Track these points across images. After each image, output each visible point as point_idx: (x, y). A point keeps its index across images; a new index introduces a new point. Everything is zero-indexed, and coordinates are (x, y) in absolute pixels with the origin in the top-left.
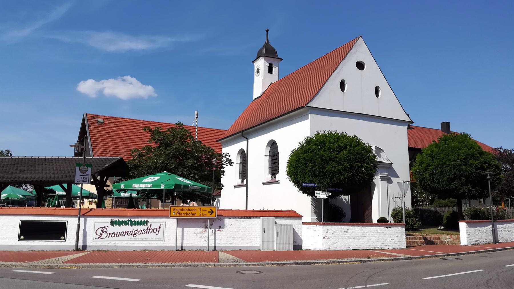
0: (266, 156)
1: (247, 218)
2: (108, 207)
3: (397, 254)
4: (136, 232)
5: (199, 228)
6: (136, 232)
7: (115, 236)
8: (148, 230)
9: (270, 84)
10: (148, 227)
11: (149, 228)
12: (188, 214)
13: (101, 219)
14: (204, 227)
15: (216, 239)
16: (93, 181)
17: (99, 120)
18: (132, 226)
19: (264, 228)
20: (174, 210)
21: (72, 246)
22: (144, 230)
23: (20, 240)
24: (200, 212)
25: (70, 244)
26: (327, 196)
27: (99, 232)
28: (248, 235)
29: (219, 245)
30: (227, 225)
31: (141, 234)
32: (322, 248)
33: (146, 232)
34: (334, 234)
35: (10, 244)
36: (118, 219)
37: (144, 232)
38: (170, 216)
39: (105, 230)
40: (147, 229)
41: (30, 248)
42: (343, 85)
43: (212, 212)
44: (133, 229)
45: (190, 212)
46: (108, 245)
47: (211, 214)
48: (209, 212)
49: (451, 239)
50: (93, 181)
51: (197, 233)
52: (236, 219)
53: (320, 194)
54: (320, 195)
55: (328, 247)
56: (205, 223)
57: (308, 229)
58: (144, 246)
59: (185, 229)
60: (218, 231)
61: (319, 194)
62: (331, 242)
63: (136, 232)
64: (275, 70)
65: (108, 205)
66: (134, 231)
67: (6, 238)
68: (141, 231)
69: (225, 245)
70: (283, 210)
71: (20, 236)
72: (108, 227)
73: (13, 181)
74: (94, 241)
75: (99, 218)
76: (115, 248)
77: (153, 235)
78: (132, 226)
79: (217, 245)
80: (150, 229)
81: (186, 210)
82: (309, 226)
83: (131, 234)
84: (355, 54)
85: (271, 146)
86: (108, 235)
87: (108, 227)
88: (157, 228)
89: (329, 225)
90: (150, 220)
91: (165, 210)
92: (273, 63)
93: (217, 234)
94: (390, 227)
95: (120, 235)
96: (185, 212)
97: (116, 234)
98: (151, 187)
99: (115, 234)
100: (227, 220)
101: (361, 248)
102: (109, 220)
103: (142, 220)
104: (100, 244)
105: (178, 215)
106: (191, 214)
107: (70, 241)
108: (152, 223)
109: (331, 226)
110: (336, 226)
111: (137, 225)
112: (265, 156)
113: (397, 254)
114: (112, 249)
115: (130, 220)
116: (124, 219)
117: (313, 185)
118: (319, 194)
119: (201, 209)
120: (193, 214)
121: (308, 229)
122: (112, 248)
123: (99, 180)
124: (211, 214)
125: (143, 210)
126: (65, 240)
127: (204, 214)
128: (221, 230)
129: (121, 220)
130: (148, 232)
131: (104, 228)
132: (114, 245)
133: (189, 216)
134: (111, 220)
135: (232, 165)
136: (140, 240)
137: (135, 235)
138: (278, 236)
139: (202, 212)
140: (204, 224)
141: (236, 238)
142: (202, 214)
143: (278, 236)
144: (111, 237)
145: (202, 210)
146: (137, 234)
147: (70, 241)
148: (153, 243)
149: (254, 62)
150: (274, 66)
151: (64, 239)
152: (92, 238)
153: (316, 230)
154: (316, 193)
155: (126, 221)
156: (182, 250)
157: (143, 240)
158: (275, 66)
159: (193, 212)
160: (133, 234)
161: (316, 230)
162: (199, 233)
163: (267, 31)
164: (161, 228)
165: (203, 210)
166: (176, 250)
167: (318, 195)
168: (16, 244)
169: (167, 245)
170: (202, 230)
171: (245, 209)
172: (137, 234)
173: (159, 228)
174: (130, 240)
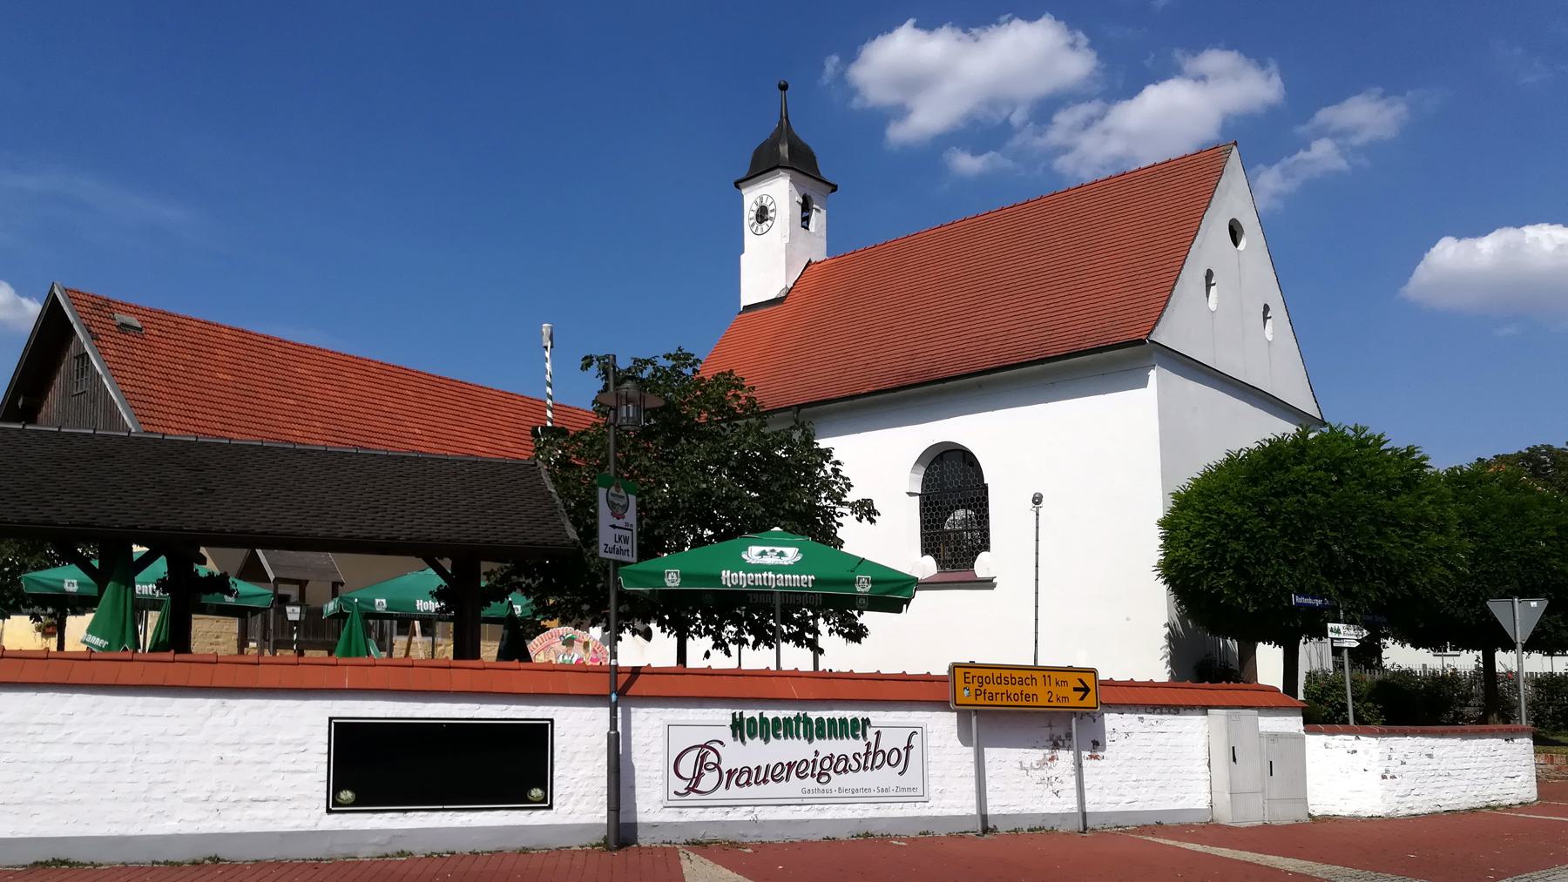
0: (910, 494)
1: (1169, 713)
2: (213, 646)
4: (828, 761)
5: (1035, 747)
6: (828, 761)
7: (752, 781)
8: (871, 757)
9: (807, 265)
10: (868, 745)
11: (872, 750)
12: (1012, 697)
13: (691, 710)
14: (1047, 744)
15: (1086, 786)
16: (134, 546)
17: (121, 318)
18: (810, 740)
19: (1233, 748)
20: (967, 680)
21: (597, 826)
22: (857, 757)
23: (334, 805)
24: (1048, 688)
25: (569, 821)
26: (1357, 640)
27: (687, 767)
28: (1174, 772)
29: (1098, 811)
30: (1115, 736)
31: (845, 770)
32: (1380, 811)
33: (862, 761)
34: (1405, 763)
35: (288, 826)
36: (761, 711)
37: (855, 766)
38: (1097, 708)
39: (712, 757)
40: (867, 754)
41: (390, 843)
43: (1086, 690)
44: (816, 752)
45: (1017, 689)
46: (724, 819)
47: (1082, 699)
48: (1076, 689)
49: (1549, 766)
50: (134, 546)
51: (1027, 765)
52: (1140, 716)
53: (1342, 631)
54: (1341, 636)
55: (1396, 805)
56: (1049, 728)
57: (1326, 748)
58: (860, 821)
59: (991, 754)
60: (1091, 757)
61: (1338, 631)
62: (1401, 790)
63: (827, 764)
64: (818, 219)
65: (214, 640)
66: (819, 759)
67: (265, 801)
68: (847, 760)
69: (1113, 810)
70: (1115, 679)
71: (336, 792)
72: (721, 743)
73: (103, 527)
74: (670, 803)
75: (685, 710)
76: (756, 832)
77: (886, 776)
78: (810, 740)
79: (1089, 808)
80: (876, 754)
81: (1003, 681)
82: (1331, 737)
83: (809, 771)
85: (931, 463)
86: (725, 776)
87: (721, 743)
88: (902, 745)
89: (1391, 734)
90: (877, 717)
91: (486, 666)
92: (814, 197)
93: (1085, 771)
94: (1513, 736)
95: (769, 778)
96: (1003, 688)
97: (755, 772)
98: (810, 586)
99: (750, 772)
100: (1112, 720)
101: (1463, 806)
102: (724, 715)
103: (849, 715)
104: (692, 815)
105: (981, 700)
106: (1022, 694)
107: (569, 807)
108: (881, 729)
109: (1397, 738)
110: (1408, 738)
111: (830, 737)
112: (908, 493)
114: (743, 835)
115: (805, 715)
116: (782, 714)
117: (1318, 602)
118: (1338, 631)
119: (1049, 676)
120: (1027, 696)
121: (1326, 748)
122: (741, 832)
123: (145, 549)
124: (1082, 699)
125: (305, 661)
126: (546, 803)
127: (1060, 695)
128: (1100, 754)
129: (770, 714)
130: (869, 764)
131: (706, 750)
132: (748, 818)
133: (1016, 703)
134: (734, 715)
135: (874, 521)
136: (845, 795)
137: (827, 778)
139: (1054, 688)
140: (1046, 732)
141: (1145, 783)
142: (1054, 698)
144: (737, 784)
145: (1053, 682)
146: (831, 772)
147: (569, 807)
148: (889, 807)
149: (741, 185)
150: (814, 206)
151: (545, 801)
152: (659, 793)
153: (1355, 752)
154: (1332, 631)
155: (787, 721)
156: (986, 830)
157: (853, 795)
158: (817, 207)
159: (1027, 690)
160: (817, 772)
161: (1355, 752)
162: (1034, 765)
163: (784, 87)
164: (912, 747)
165: (1057, 683)
166: (980, 832)
167: (1337, 636)
168: (320, 828)
169: (935, 812)
170: (1045, 755)
171: (810, 668)
172: (831, 772)
173: (908, 747)
174: (807, 795)
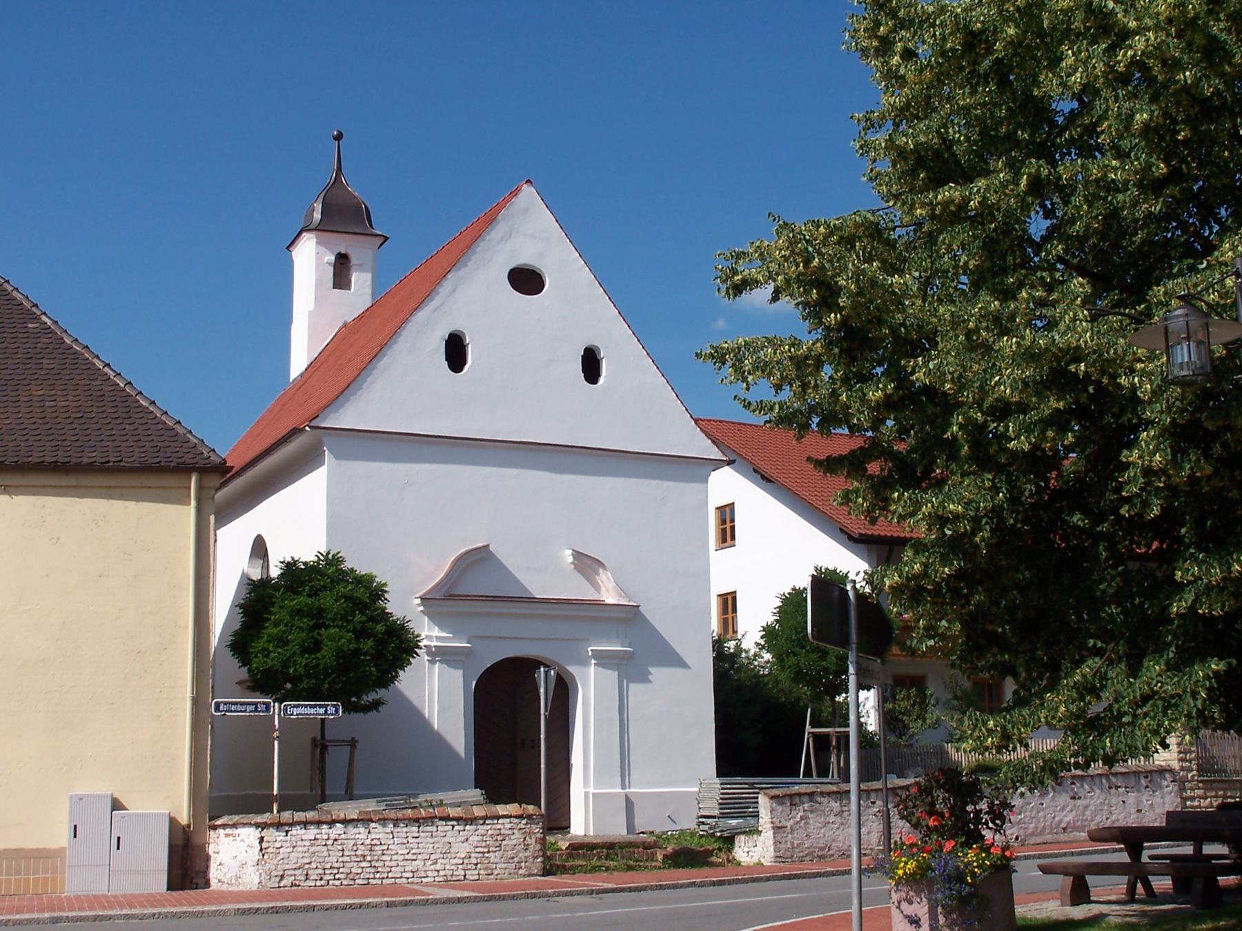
3: (600, 884)
19: (75, 826)
42: (456, 351)
64: (360, 280)
84: (506, 241)
113: (600, 884)
138: (118, 848)
143: (118, 848)
163: (339, 137)
